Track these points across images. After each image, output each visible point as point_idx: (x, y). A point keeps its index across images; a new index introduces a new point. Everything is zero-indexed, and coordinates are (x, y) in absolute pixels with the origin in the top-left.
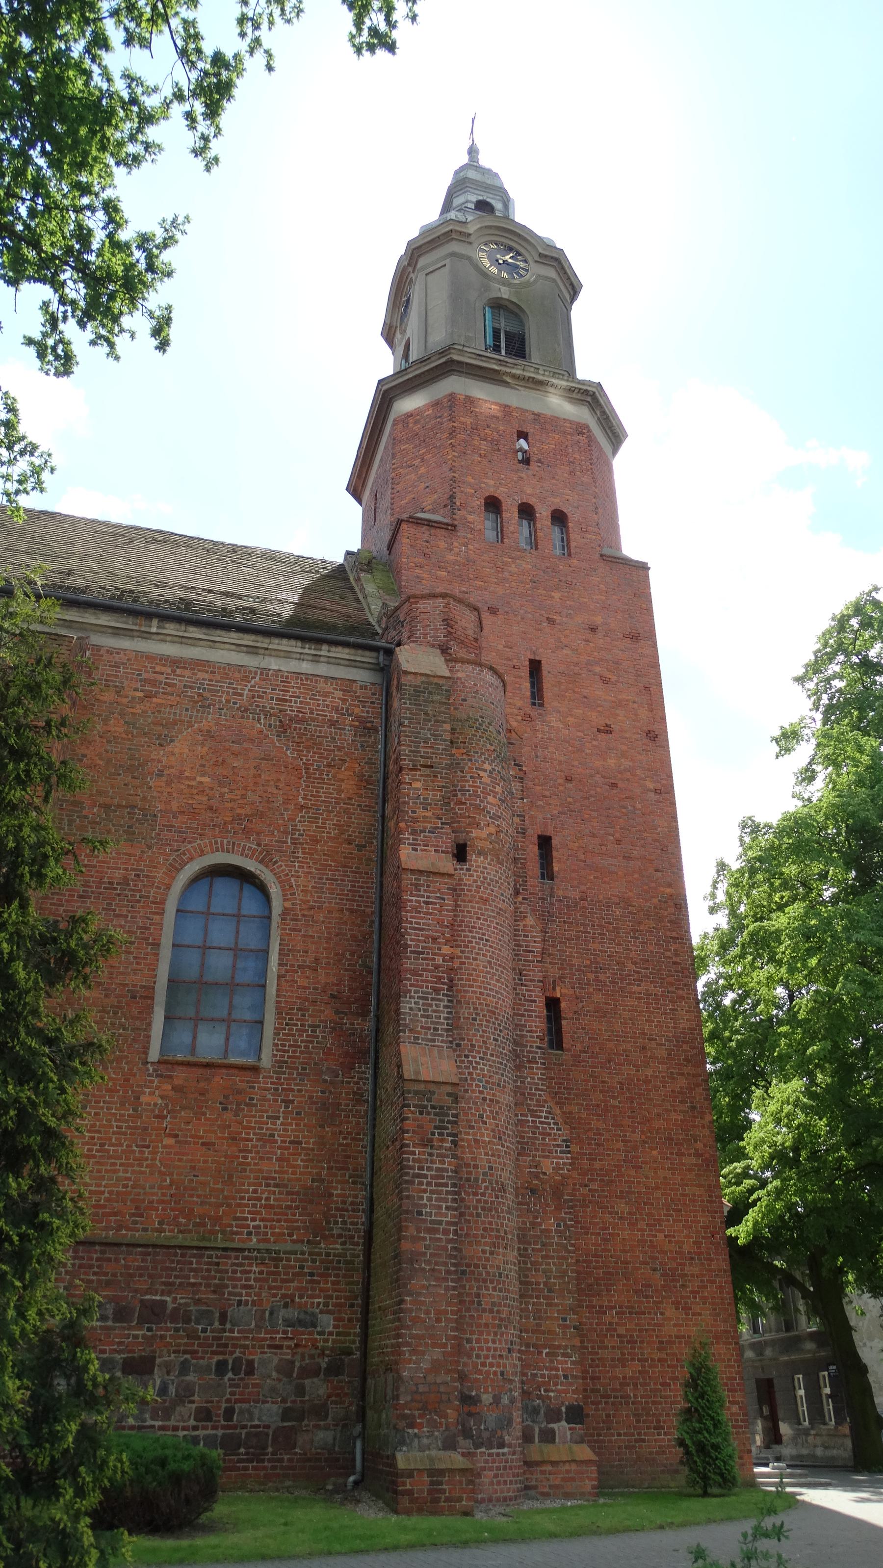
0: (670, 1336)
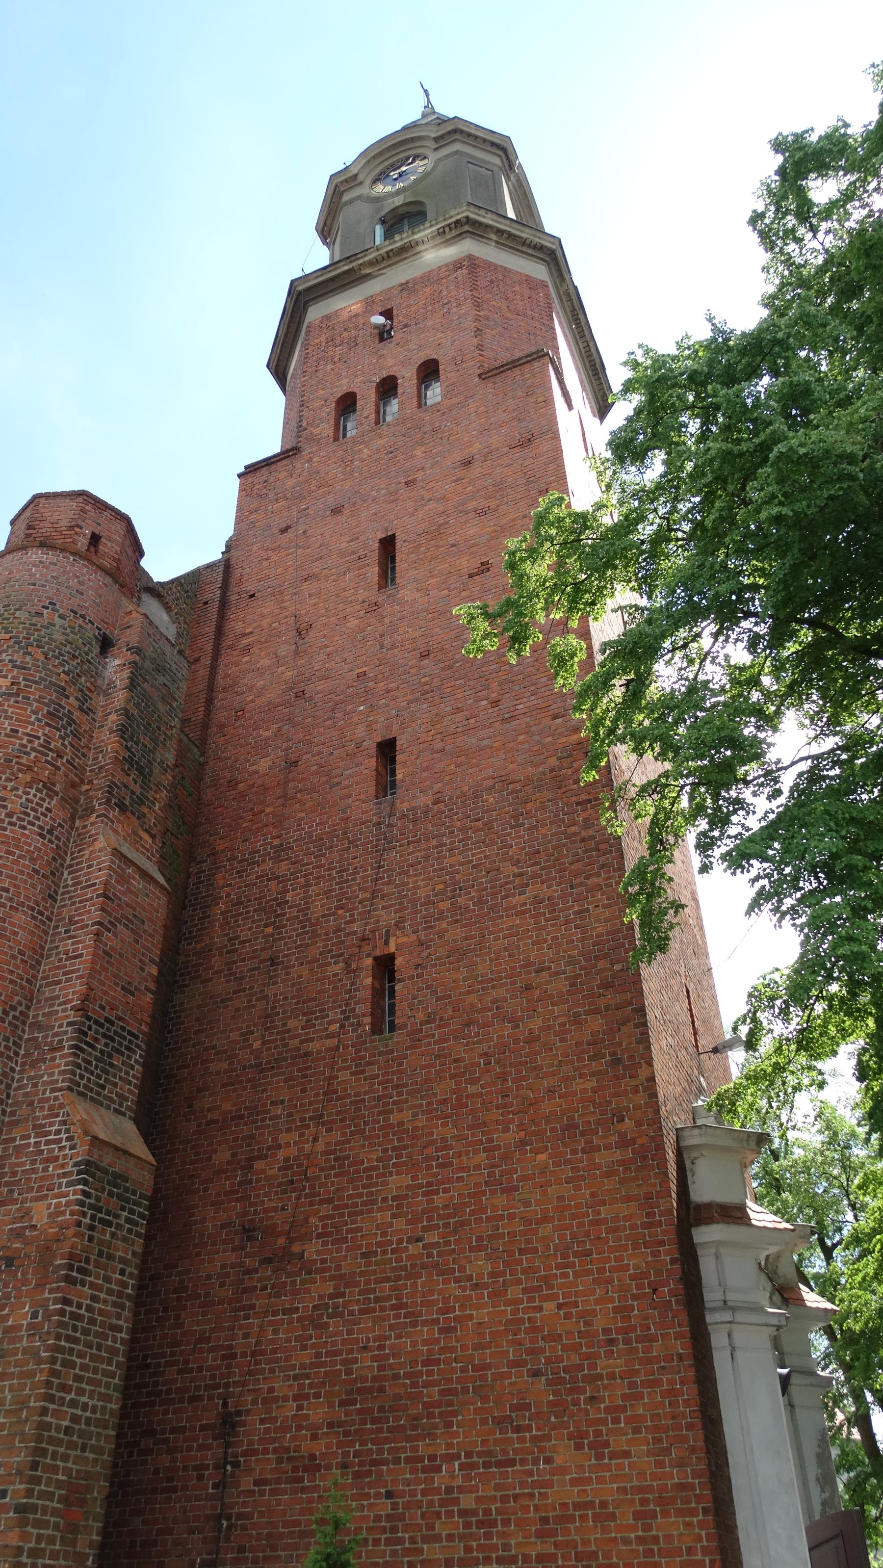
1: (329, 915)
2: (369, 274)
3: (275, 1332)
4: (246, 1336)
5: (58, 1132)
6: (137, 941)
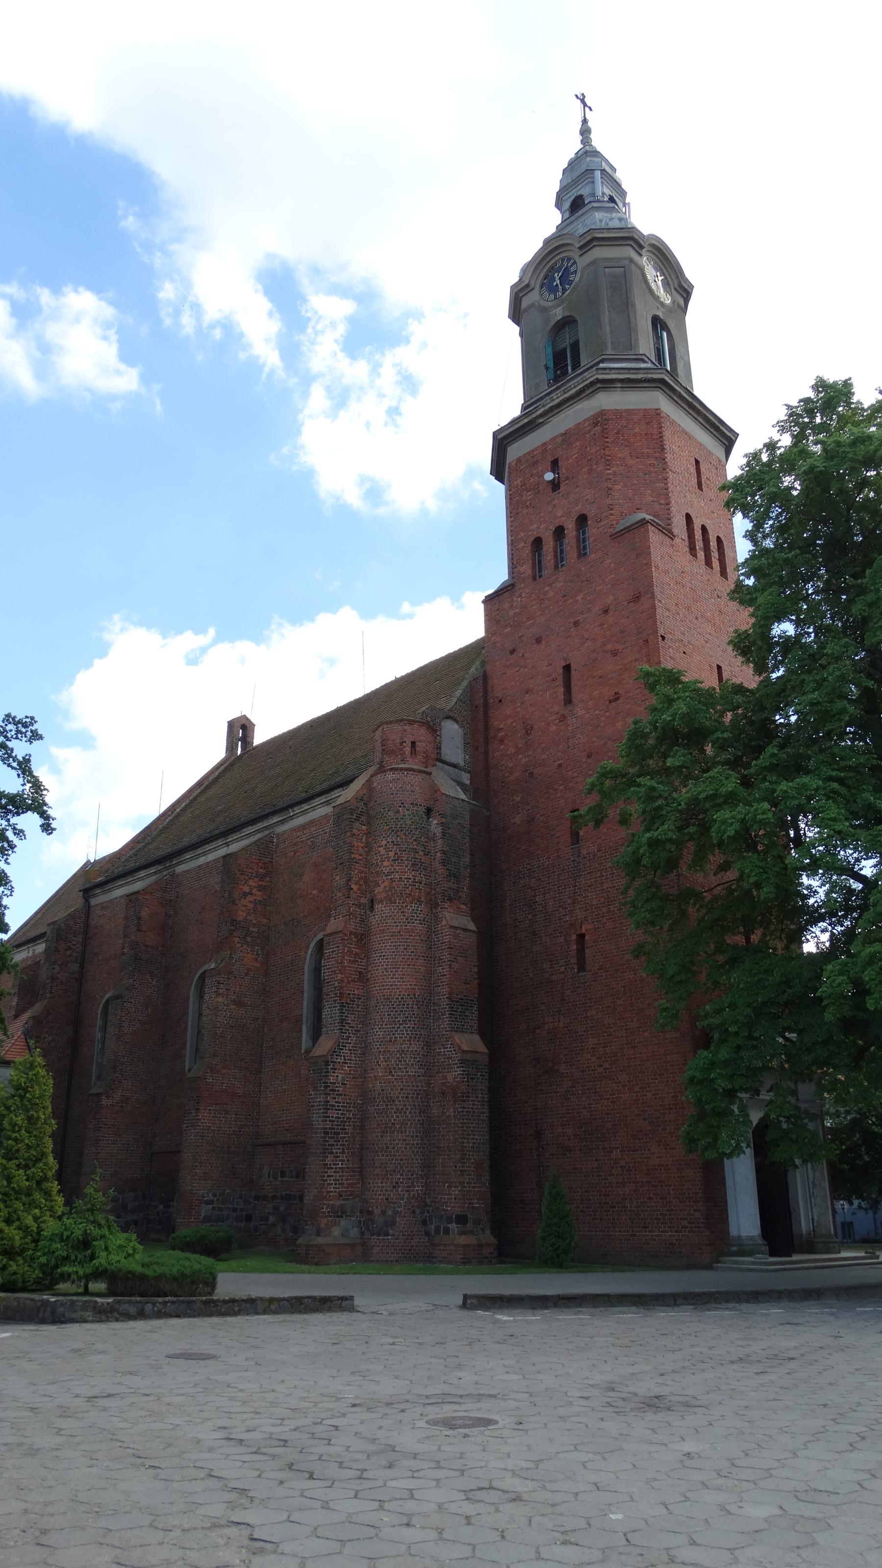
0: (654, 1165)
2: (542, 422)
3: (552, 1100)
4: (541, 1101)
5: (450, 1048)
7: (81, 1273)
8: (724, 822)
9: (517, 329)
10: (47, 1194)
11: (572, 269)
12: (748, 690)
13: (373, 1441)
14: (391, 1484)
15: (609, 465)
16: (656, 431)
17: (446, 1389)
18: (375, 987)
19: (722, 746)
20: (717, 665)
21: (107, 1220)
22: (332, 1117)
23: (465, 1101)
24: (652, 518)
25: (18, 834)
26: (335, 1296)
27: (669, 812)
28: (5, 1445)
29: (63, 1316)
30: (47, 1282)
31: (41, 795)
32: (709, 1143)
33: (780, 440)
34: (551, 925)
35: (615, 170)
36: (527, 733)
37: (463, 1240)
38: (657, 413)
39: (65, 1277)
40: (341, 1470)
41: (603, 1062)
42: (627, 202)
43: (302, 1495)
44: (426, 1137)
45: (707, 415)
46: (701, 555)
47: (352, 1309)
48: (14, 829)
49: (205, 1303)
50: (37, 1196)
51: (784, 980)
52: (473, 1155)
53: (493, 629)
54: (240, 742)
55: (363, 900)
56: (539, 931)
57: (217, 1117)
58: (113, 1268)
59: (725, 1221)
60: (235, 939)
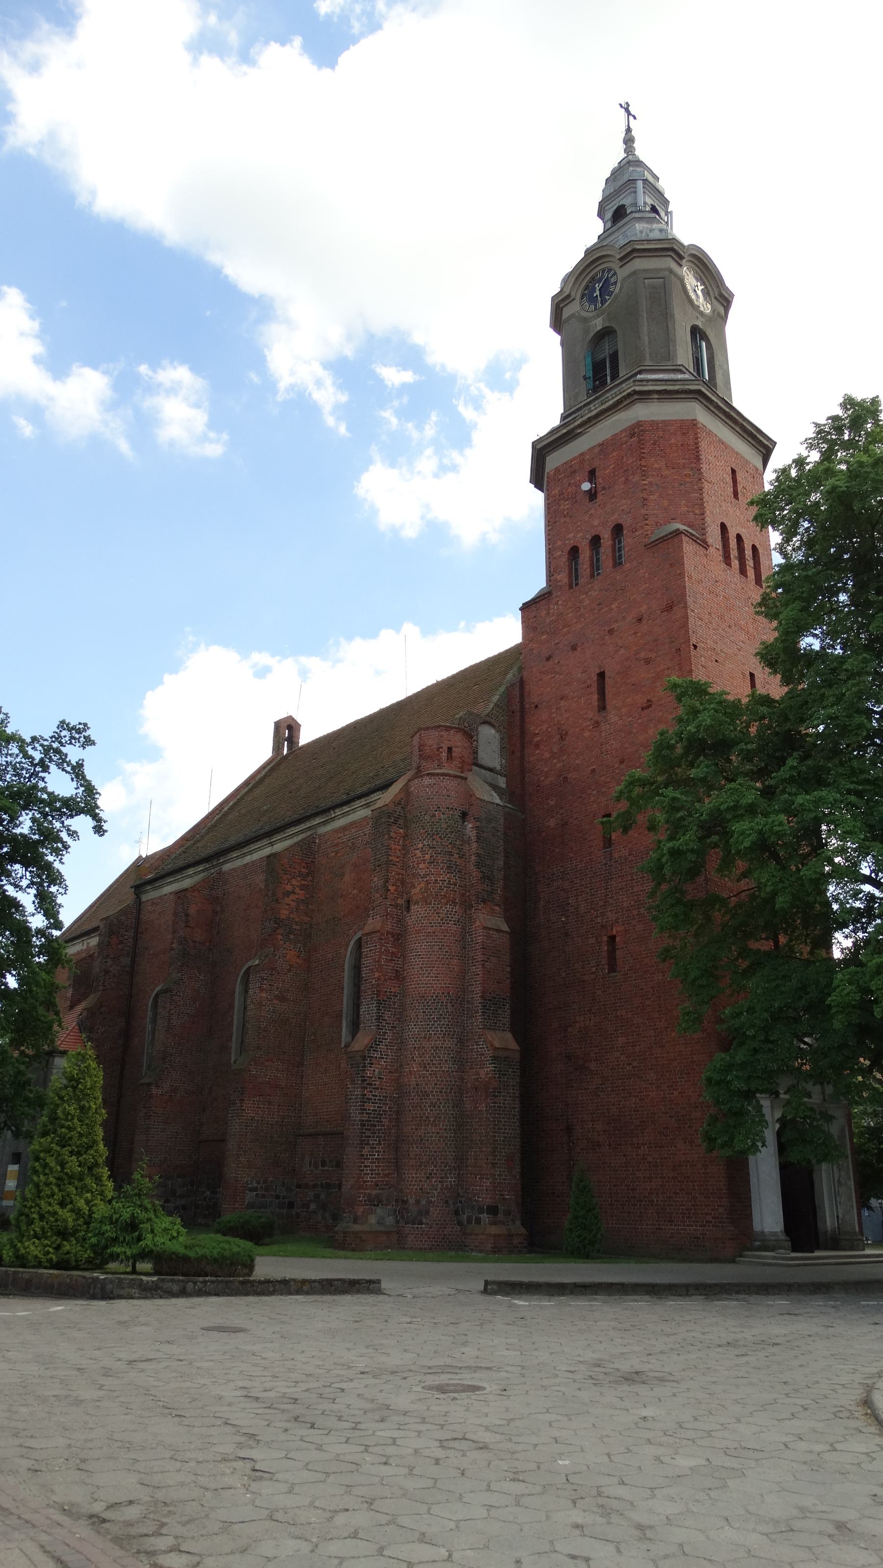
1: (587, 912)
3: (582, 1096)
6: (499, 961)
7: (129, 1253)
8: (742, 833)
9: (557, 338)
10: (98, 1179)
11: (612, 280)
12: (774, 701)
13: (372, 1401)
14: (378, 1433)
15: (645, 476)
16: (691, 442)
17: (449, 1361)
18: (411, 985)
19: (748, 757)
20: (750, 673)
21: (153, 1205)
22: (369, 1110)
23: (496, 1096)
24: (686, 528)
25: (72, 835)
26: (364, 1280)
27: (691, 822)
28: (55, 1396)
29: (112, 1292)
30: (98, 1261)
31: (94, 799)
32: (725, 1141)
33: (809, 456)
34: (583, 926)
35: (658, 179)
36: (562, 738)
37: (494, 1230)
38: (694, 424)
39: (114, 1257)
40: (339, 1422)
41: (632, 1060)
42: (669, 210)
43: (301, 1440)
44: (459, 1130)
45: (745, 424)
46: (735, 563)
47: (379, 1292)
48: (68, 830)
49: (242, 1283)
50: (88, 1181)
51: (800, 986)
52: (504, 1149)
53: (530, 636)
54: (286, 742)
55: (400, 901)
56: (571, 932)
57: (260, 1108)
58: (158, 1249)
59: (749, 1217)
60: (278, 936)
